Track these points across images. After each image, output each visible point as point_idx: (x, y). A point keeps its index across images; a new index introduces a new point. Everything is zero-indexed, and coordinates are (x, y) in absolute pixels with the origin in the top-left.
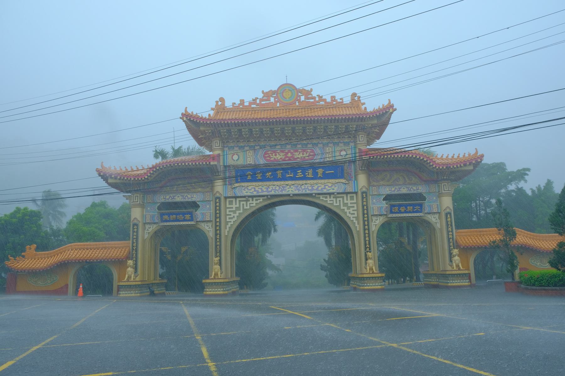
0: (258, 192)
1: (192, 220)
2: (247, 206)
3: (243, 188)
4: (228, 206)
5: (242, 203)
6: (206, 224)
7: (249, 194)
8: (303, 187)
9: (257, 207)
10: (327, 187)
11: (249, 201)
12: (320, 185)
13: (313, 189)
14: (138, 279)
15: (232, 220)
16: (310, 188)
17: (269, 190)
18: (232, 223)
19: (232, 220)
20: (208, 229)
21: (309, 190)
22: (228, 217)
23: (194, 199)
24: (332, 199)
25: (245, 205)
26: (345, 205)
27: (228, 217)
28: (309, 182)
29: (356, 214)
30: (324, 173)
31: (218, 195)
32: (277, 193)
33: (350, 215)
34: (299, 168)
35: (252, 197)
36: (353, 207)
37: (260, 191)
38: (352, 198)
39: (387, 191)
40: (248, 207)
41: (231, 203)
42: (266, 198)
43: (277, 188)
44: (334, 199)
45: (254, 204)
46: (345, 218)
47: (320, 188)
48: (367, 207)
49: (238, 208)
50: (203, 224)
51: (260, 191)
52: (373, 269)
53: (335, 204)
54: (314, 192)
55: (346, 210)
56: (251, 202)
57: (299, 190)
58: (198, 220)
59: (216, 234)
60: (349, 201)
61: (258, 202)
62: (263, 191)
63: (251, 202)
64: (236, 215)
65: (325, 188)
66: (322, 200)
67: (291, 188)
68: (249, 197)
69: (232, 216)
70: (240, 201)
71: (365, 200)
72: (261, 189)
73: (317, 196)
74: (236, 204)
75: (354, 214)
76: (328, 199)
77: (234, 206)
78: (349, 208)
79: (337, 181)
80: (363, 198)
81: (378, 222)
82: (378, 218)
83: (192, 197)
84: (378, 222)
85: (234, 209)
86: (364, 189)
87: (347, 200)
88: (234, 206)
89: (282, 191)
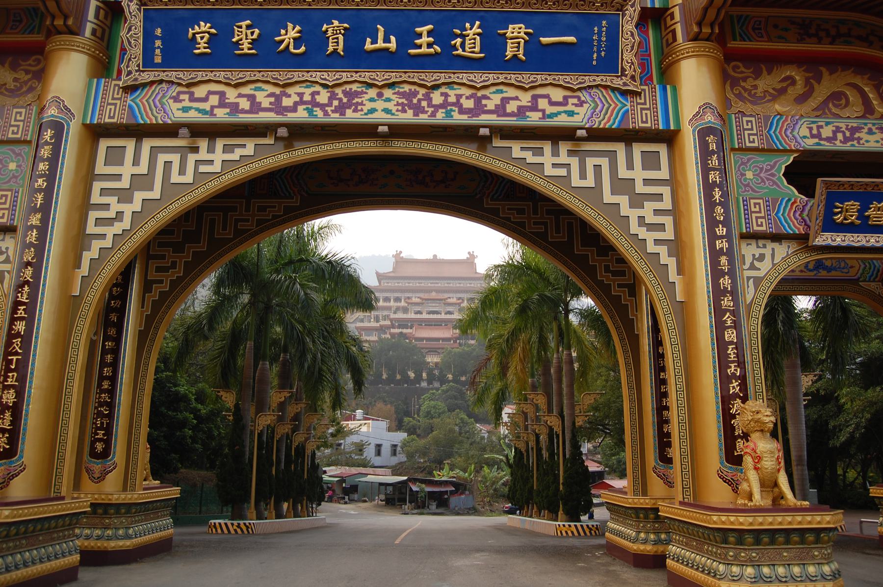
0: (235, 108)
2: (182, 172)
5: (162, 158)
7: (193, 116)
8: (437, 98)
9: (229, 179)
10: (543, 103)
11: (195, 150)
12: (511, 92)
13: (479, 109)
15: (110, 231)
17: (287, 102)
18: (108, 243)
19: (110, 231)
21: (462, 111)
26: (622, 186)
27: (93, 215)
30: (532, 43)
33: (643, 233)
36: (659, 197)
37: (245, 104)
39: (807, 133)
40: (188, 178)
41: (115, 157)
43: (323, 97)
44: (574, 162)
45: (220, 164)
47: (512, 107)
48: (725, 195)
49: (141, 182)
51: (245, 104)
52: (776, 484)
53: (576, 181)
54: (484, 118)
55: (625, 210)
56: (203, 155)
57: (418, 110)
60: (639, 174)
62: (256, 107)
64: (128, 209)
65: (534, 108)
66: (520, 161)
69: (111, 214)
70: (154, 151)
71: (714, 161)
72: (251, 98)
73: (497, 143)
74: (136, 162)
75: (661, 227)
77: (127, 170)
78: (637, 201)
79: (589, 79)
82: (767, 252)
84: (765, 267)
85: (125, 183)
86: (710, 119)
87: (630, 166)
88: (127, 170)
89: (341, 109)
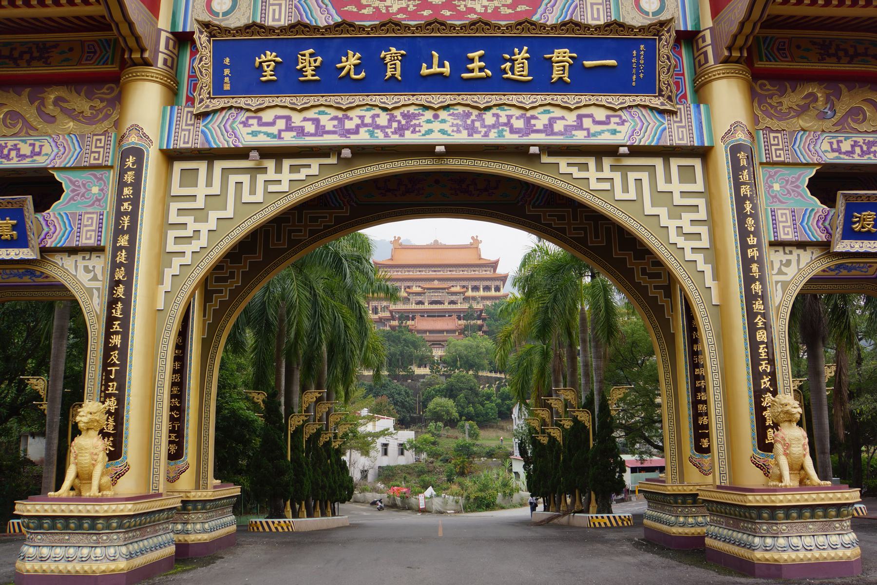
0: (301, 131)
1: (21, 241)
2: (253, 192)
3: (243, 116)
4: (176, 190)
5: (233, 179)
6: (81, 263)
7: (263, 140)
10: (587, 123)
11: (264, 170)
12: (557, 113)
13: (529, 129)
14: (128, 485)
16: (519, 124)
17: (349, 125)
18: (187, 260)
19: (188, 249)
20: (85, 280)
21: (513, 131)
22: (172, 234)
23: (41, 162)
24: (607, 173)
25: (246, 187)
26: (662, 197)
27: (172, 234)
28: (514, 98)
29: (705, 236)
30: (576, 67)
31: (133, 140)
32: (380, 139)
33: (681, 242)
34: (475, 43)
35: (277, 154)
37: (310, 127)
38: (687, 174)
40: (259, 197)
41: (189, 177)
42: (333, 160)
44: (617, 176)
45: (288, 185)
46: (663, 253)
47: (559, 126)
50: (68, 262)
51: (310, 127)
52: (802, 468)
53: (619, 195)
54: (534, 138)
56: (271, 175)
57: (472, 130)
58: (50, 243)
59: (112, 303)
60: (676, 187)
61: (302, 175)
62: (320, 130)
63: (271, 175)
64: (204, 228)
65: (580, 127)
67: (440, 125)
68: (266, 153)
69: (189, 233)
72: (316, 121)
73: (545, 159)
74: (209, 183)
76: (592, 173)
78: (676, 211)
79: (629, 100)
80: (736, 169)
81: (791, 272)
82: (793, 257)
83: (34, 154)
84: (791, 272)
85: (200, 203)
86: (741, 137)
87: (668, 180)
88: (201, 190)
89: (400, 130)
